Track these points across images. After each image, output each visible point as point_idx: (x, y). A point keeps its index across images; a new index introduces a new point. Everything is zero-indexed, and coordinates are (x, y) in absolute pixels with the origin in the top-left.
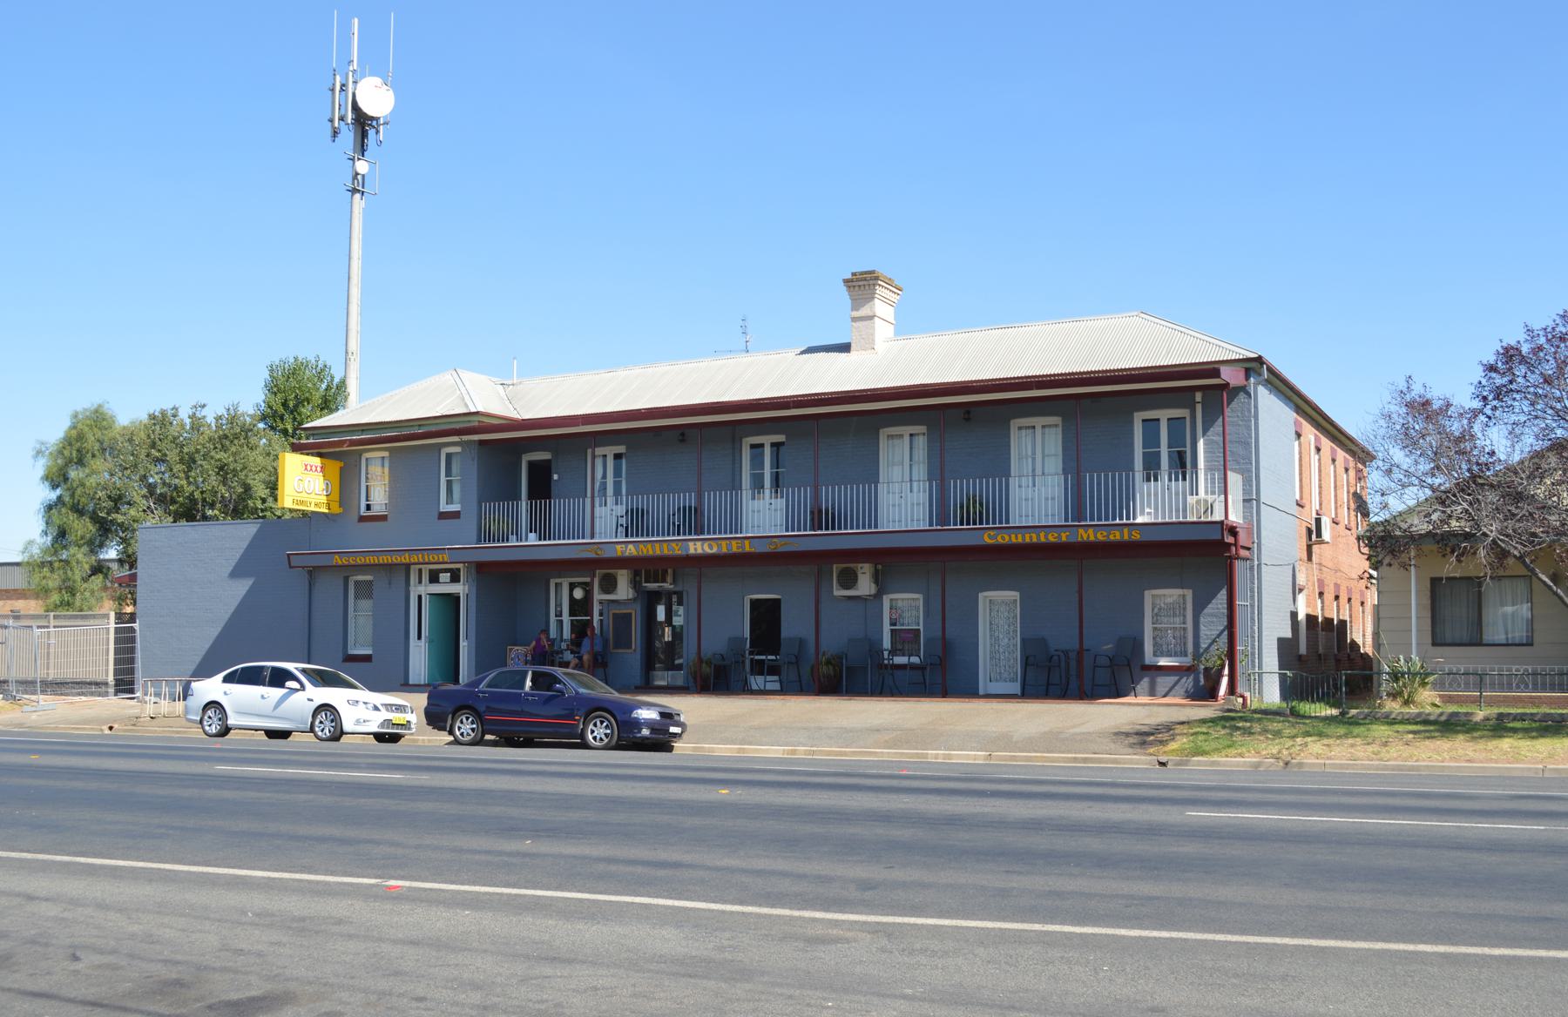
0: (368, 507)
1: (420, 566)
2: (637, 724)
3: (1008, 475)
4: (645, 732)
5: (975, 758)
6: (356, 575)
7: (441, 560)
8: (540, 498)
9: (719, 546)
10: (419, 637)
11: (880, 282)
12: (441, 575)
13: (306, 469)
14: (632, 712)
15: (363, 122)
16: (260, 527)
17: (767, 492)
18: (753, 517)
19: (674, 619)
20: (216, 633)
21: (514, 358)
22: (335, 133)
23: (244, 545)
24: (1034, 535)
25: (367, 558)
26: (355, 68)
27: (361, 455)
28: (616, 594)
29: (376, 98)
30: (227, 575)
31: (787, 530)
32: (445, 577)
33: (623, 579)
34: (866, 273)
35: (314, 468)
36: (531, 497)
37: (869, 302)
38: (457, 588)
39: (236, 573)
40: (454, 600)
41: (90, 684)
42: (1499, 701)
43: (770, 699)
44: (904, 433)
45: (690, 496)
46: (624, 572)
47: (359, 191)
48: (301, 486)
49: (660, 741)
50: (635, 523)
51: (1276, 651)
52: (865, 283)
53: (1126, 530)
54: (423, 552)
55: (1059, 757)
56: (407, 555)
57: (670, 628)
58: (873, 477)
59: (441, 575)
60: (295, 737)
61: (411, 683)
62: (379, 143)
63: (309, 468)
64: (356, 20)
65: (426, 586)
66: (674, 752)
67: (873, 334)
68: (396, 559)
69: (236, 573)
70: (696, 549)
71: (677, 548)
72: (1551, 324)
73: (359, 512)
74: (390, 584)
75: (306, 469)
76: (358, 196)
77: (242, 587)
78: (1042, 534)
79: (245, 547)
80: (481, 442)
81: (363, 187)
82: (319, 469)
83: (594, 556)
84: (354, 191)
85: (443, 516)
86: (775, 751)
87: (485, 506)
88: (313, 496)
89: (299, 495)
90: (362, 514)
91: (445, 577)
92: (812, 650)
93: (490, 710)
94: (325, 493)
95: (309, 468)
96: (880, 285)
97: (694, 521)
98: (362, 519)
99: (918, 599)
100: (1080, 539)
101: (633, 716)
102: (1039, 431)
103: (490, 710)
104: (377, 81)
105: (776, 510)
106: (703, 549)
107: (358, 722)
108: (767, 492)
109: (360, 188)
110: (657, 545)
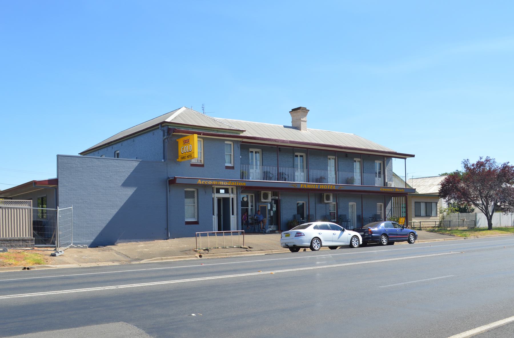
1: (233, 187)
3: (354, 172)
6: (186, 188)
7: (219, 184)
9: (307, 186)
10: (233, 214)
12: (220, 190)
13: (184, 143)
16: (139, 163)
17: (299, 170)
18: (286, 176)
19: (273, 208)
20: (115, 213)
21: (300, 119)
23: (132, 170)
24: (217, 182)
25: (243, 183)
28: (268, 200)
30: (121, 184)
32: (222, 191)
33: (270, 194)
34: (304, 108)
38: (230, 196)
39: (126, 184)
40: (226, 200)
41: (19, 240)
44: (330, 158)
45: (275, 168)
50: (266, 175)
52: (306, 111)
53: (402, 189)
54: (237, 181)
57: (272, 211)
58: (327, 170)
59: (220, 190)
68: (240, 184)
69: (126, 184)
70: (322, 187)
71: (317, 186)
72: (491, 158)
74: (206, 193)
77: (130, 191)
78: (235, 183)
79: (131, 171)
83: (294, 187)
85: (227, 167)
91: (222, 191)
92: (361, 217)
97: (280, 176)
102: (254, 153)
103: (390, 236)
105: (257, 173)
106: (201, 183)
108: (299, 170)
110: (312, 185)
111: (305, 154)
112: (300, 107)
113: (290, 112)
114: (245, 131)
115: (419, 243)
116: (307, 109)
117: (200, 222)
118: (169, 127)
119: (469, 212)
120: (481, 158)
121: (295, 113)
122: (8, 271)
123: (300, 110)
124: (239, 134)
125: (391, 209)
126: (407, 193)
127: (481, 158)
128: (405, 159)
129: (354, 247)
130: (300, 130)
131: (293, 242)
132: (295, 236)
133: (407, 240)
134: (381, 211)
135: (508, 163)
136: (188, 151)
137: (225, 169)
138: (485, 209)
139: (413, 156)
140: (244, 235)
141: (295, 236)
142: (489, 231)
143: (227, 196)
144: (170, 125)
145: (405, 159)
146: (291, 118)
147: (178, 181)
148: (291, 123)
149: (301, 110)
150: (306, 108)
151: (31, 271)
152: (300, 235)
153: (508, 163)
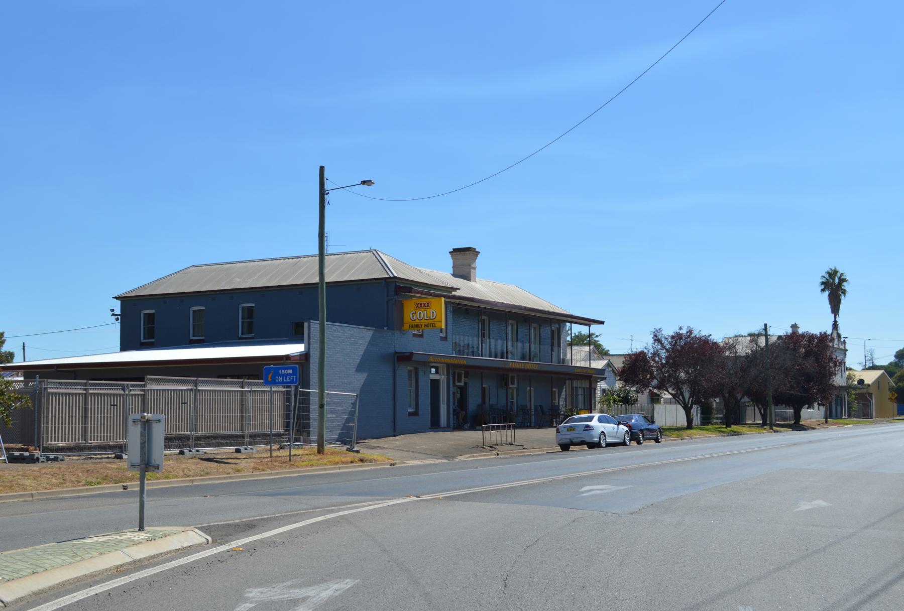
48: (415, 316)
74: (424, 373)
75: (418, 306)
88: (423, 321)
111: (515, 322)
112: (470, 248)
113: (450, 252)
114: (459, 289)
115: (274, 477)
116: (476, 250)
117: (420, 413)
118: (397, 284)
119: (632, 404)
120: (681, 328)
121: (460, 256)
122: (289, 475)
123: (469, 252)
124: (451, 292)
125: (566, 398)
126: (592, 376)
127: (681, 328)
128: (589, 326)
129: (602, 447)
130: (470, 281)
131: (581, 438)
132: (584, 430)
133: (654, 438)
134: (512, 399)
135: (710, 335)
136: (426, 318)
137: (439, 341)
138: (682, 399)
139: (602, 323)
140: (516, 430)
141: (584, 430)
142: (689, 432)
143: (437, 377)
144: (398, 282)
145: (589, 326)
146: (452, 261)
147: (414, 358)
148: (452, 269)
149: (472, 252)
150: (475, 249)
151: (397, 467)
152: (589, 429)
153: (710, 335)
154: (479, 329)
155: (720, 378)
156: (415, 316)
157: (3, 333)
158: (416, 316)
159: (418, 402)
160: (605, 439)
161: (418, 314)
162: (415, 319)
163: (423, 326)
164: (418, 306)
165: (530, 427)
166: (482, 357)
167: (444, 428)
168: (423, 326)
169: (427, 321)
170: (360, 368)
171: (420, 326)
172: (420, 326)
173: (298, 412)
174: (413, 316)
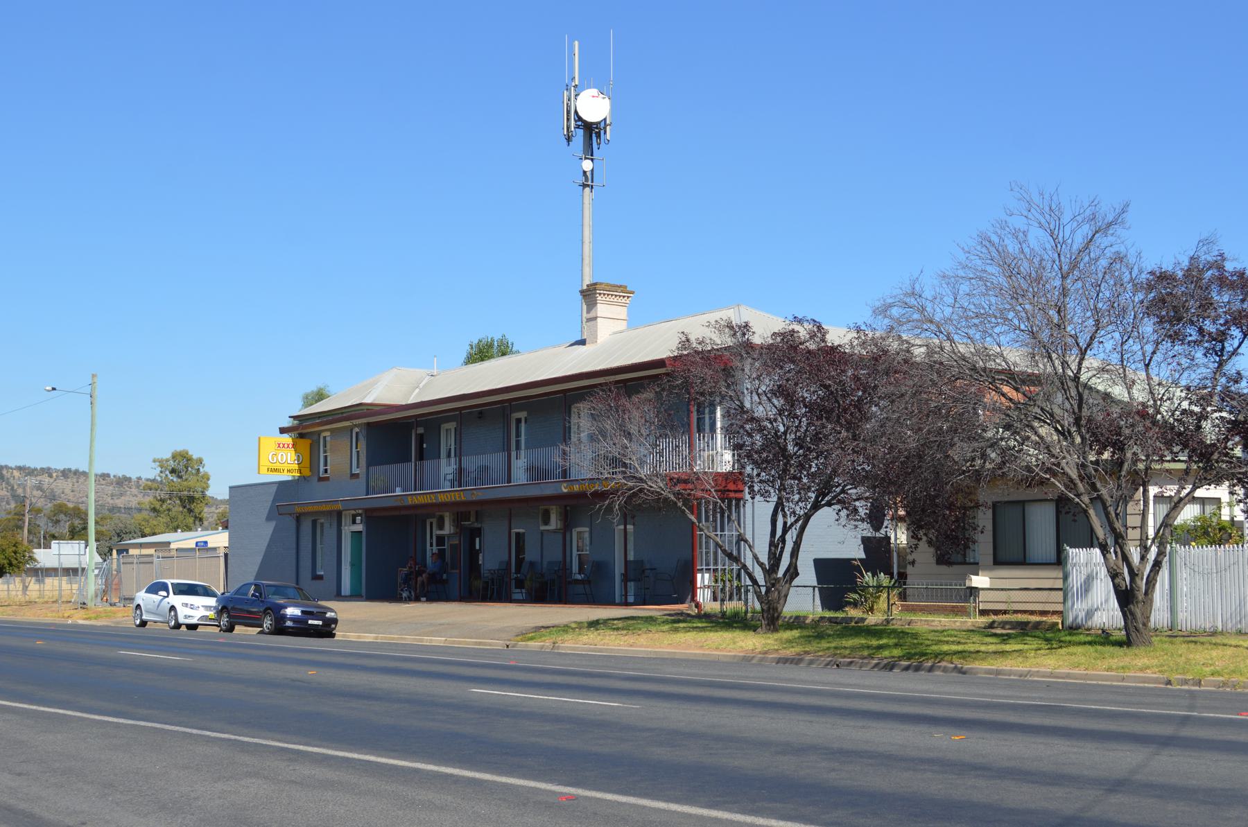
0: (326, 471)
2: (284, 617)
4: (289, 623)
5: (440, 641)
8: (429, 459)
11: (598, 292)
14: (280, 611)
15: (591, 130)
21: (435, 356)
22: (569, 139)
26: (577, 83)
27: (319, 435)
29: (593, 107)
31: (527, 481)
35: (286, 446)
36: (527, 448)
37: (594, 307)
42: (935, 610)
43: (488, 605)
46: (554, 507)
47: (588, 186)
48: (275, 459)
49: (326, 631)
51: (813, 569)
55: (470, 642)
56: (428, 496)
60: (200, 629)
61: (343, 594)
62: (607, 142)
63: (281, 446)
64: (576, 43)
65: (350, 525)
66: (146, 627)
67: (596, 331)
73: (319, 474)
74: (331, 525)
75: (279, 446)
76: (587, 190)
80: (368, 424)
81: (592, 182)
82: (291, 446)
84: (584, 186)
86: (438, 641)
87: (378, 470)
88: (286, 464)
89: (274, 465)
90: (321, 476)
93: (233, 608)
94: (296, 462)
95: (281, 446)
96: (600, 294)
98: (320, 479)
99: (579, 533)
100: (440, 500)
101: (281, 612)
104: (594, 91)
107: (186, 617)
109: (590, 183)
136: (289, 462)
150: (626, 287)
154: (504, 437)
155: (967, 486)
156: (275, 459)
157: (466, 363)
158: (277, 459)
159: (337, 560)
160: (141, 615)
161: (280, 456)
162: (275, 461)
163: (286, 471)
164: (279, 446)
165: (448, 599)
166: (415, 490)
167: (346, 596)
168: (286, 471)
169: (289, 465)
170: (269, 519)
171: (282, 471)
172: (282, 471)
173: (706, 549)
174: (273, 459)
